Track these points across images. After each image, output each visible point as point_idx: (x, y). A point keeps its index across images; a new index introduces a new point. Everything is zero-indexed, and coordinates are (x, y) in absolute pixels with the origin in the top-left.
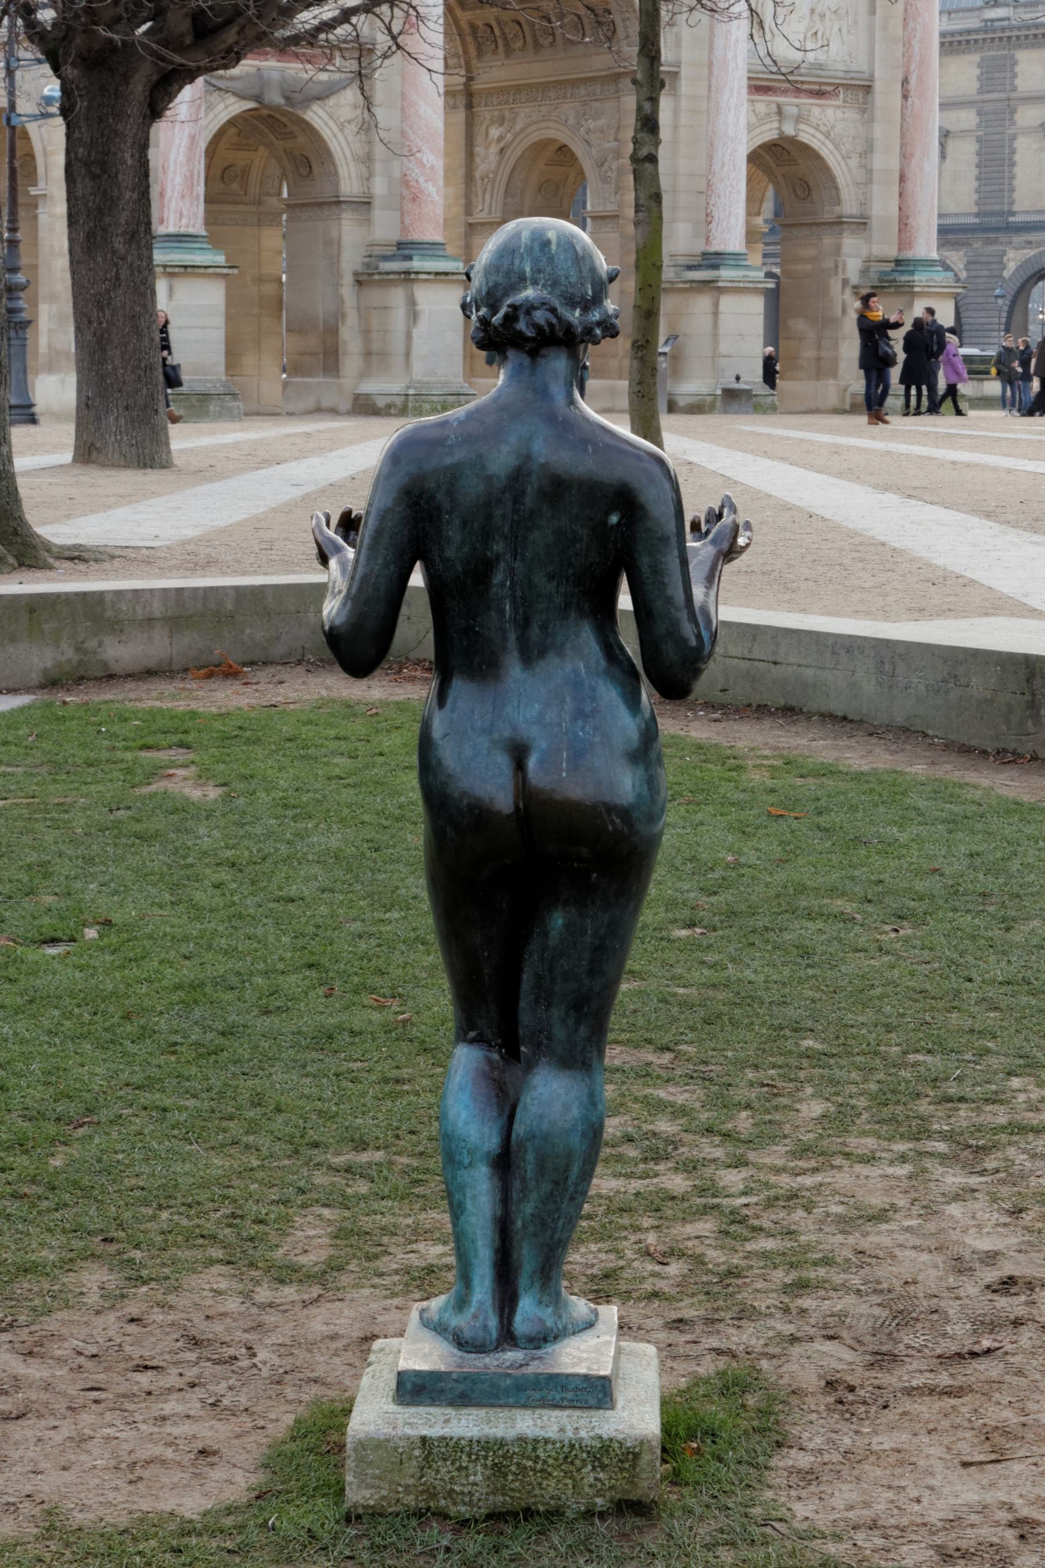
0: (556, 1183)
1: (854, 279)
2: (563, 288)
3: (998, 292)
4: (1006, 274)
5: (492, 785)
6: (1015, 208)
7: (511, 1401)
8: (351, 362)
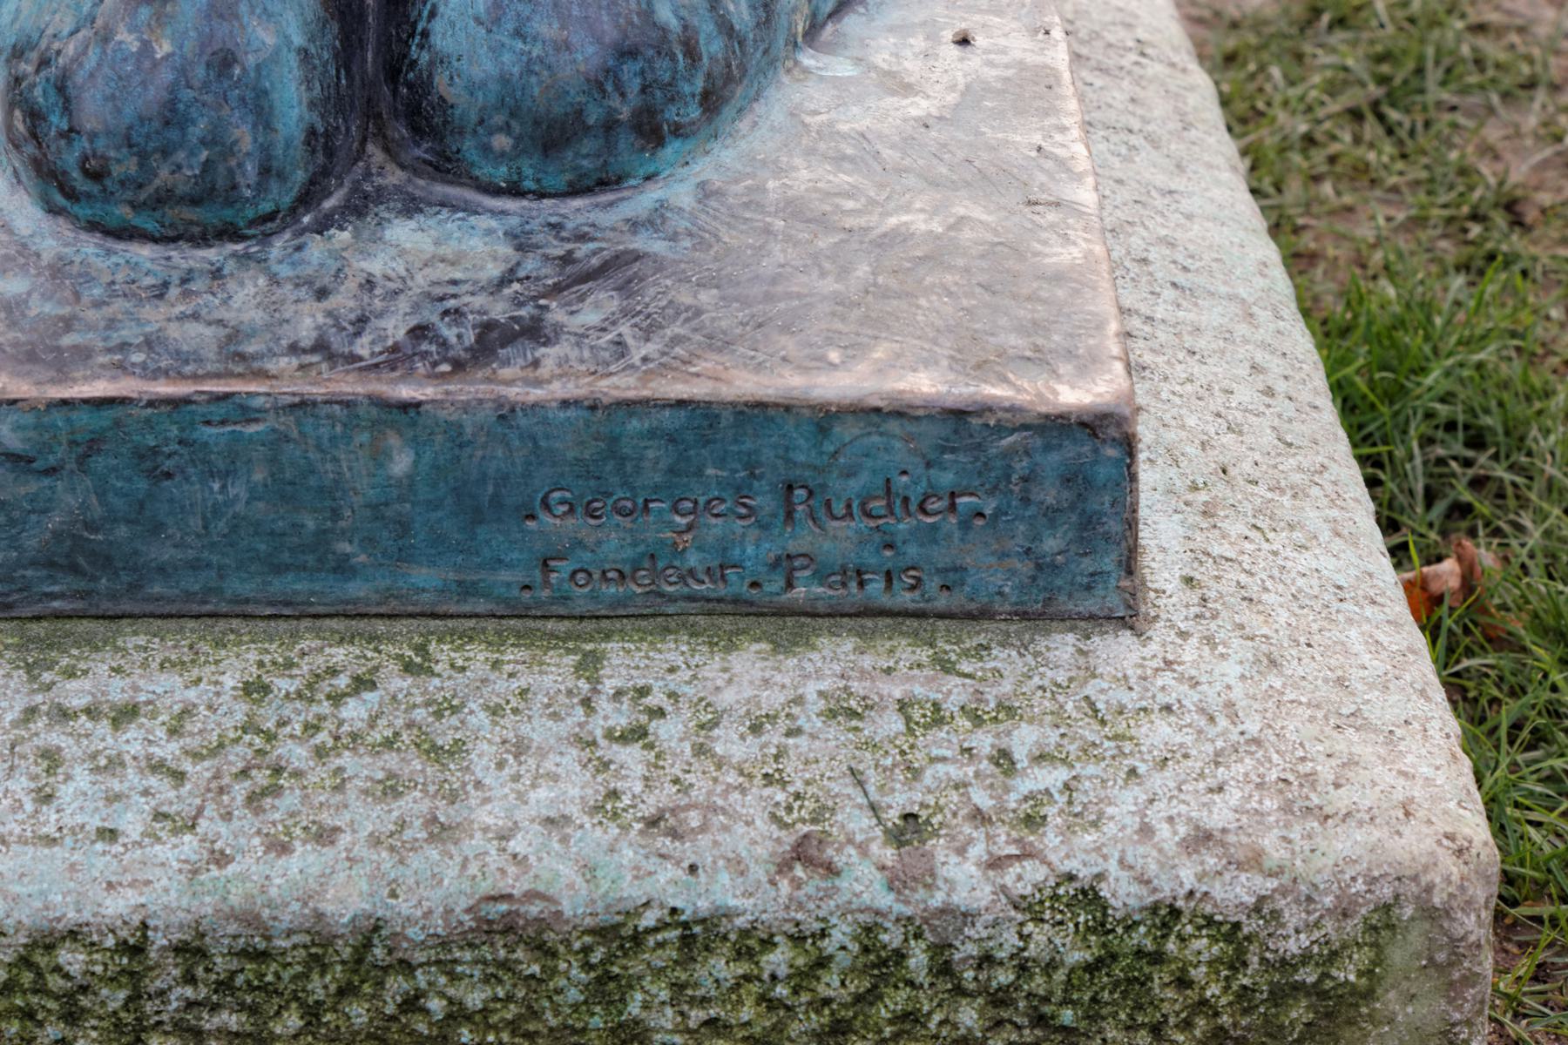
7: (425, 577)
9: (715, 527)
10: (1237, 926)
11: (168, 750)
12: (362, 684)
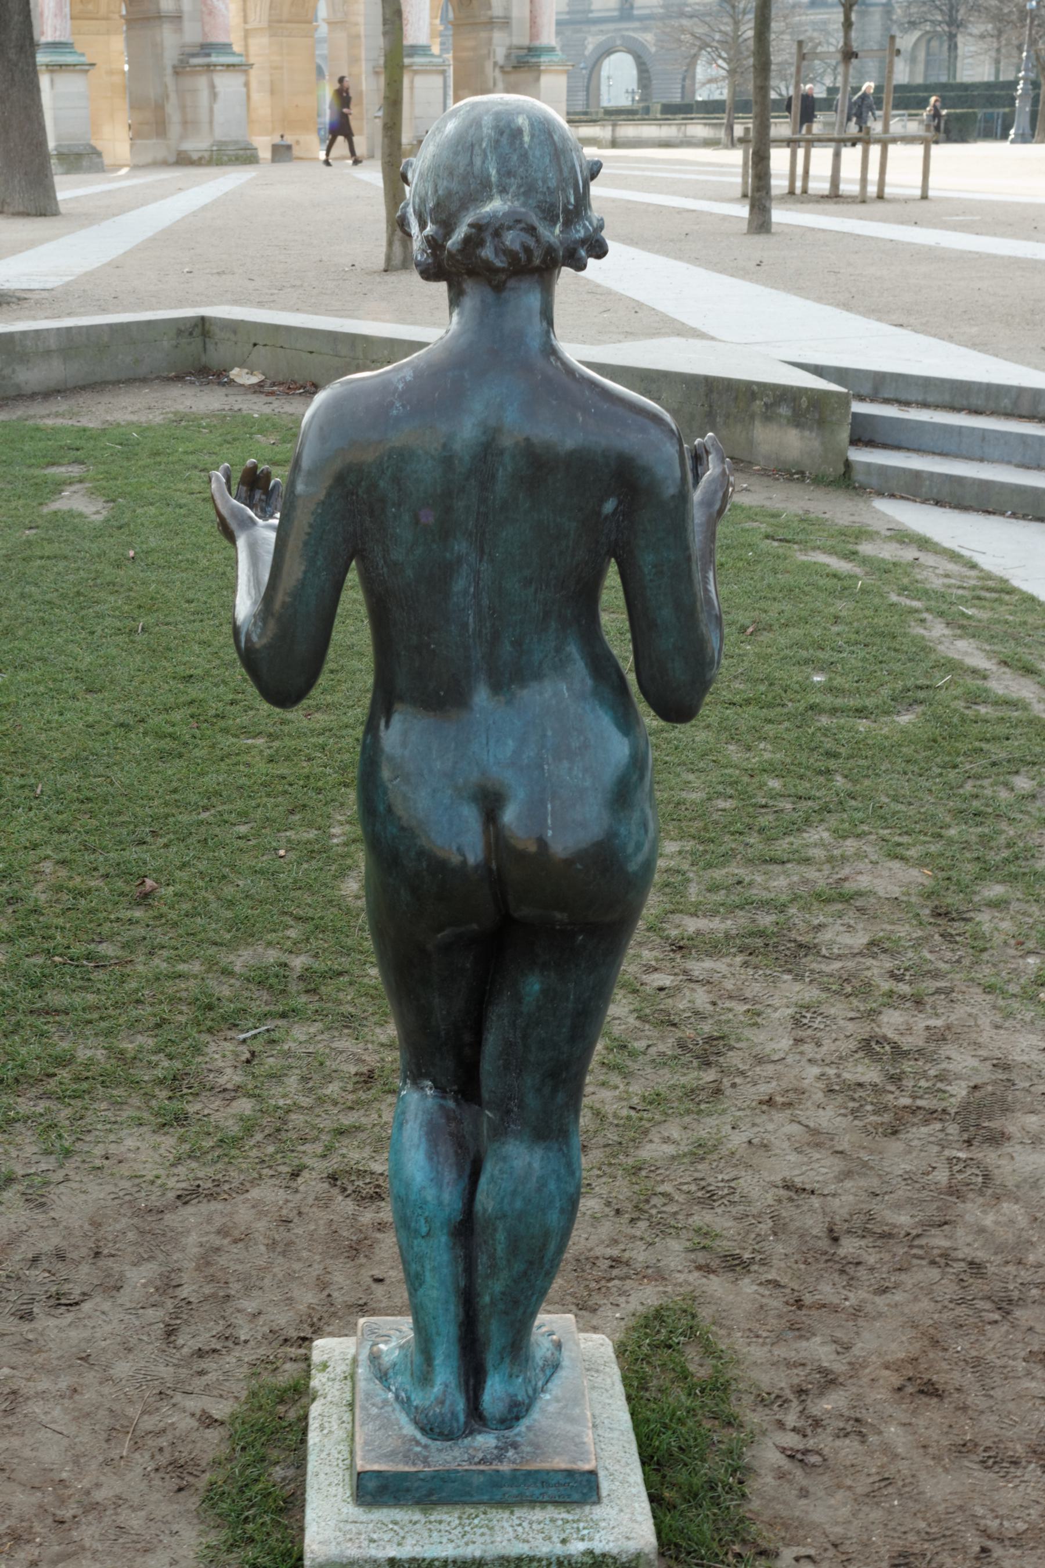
0: (531, 1263)
2: (540, 197)
4: (587, 53)
5: (458, 837)
6: (593, 7)
7: (485, 1498)
8: (175, 130)
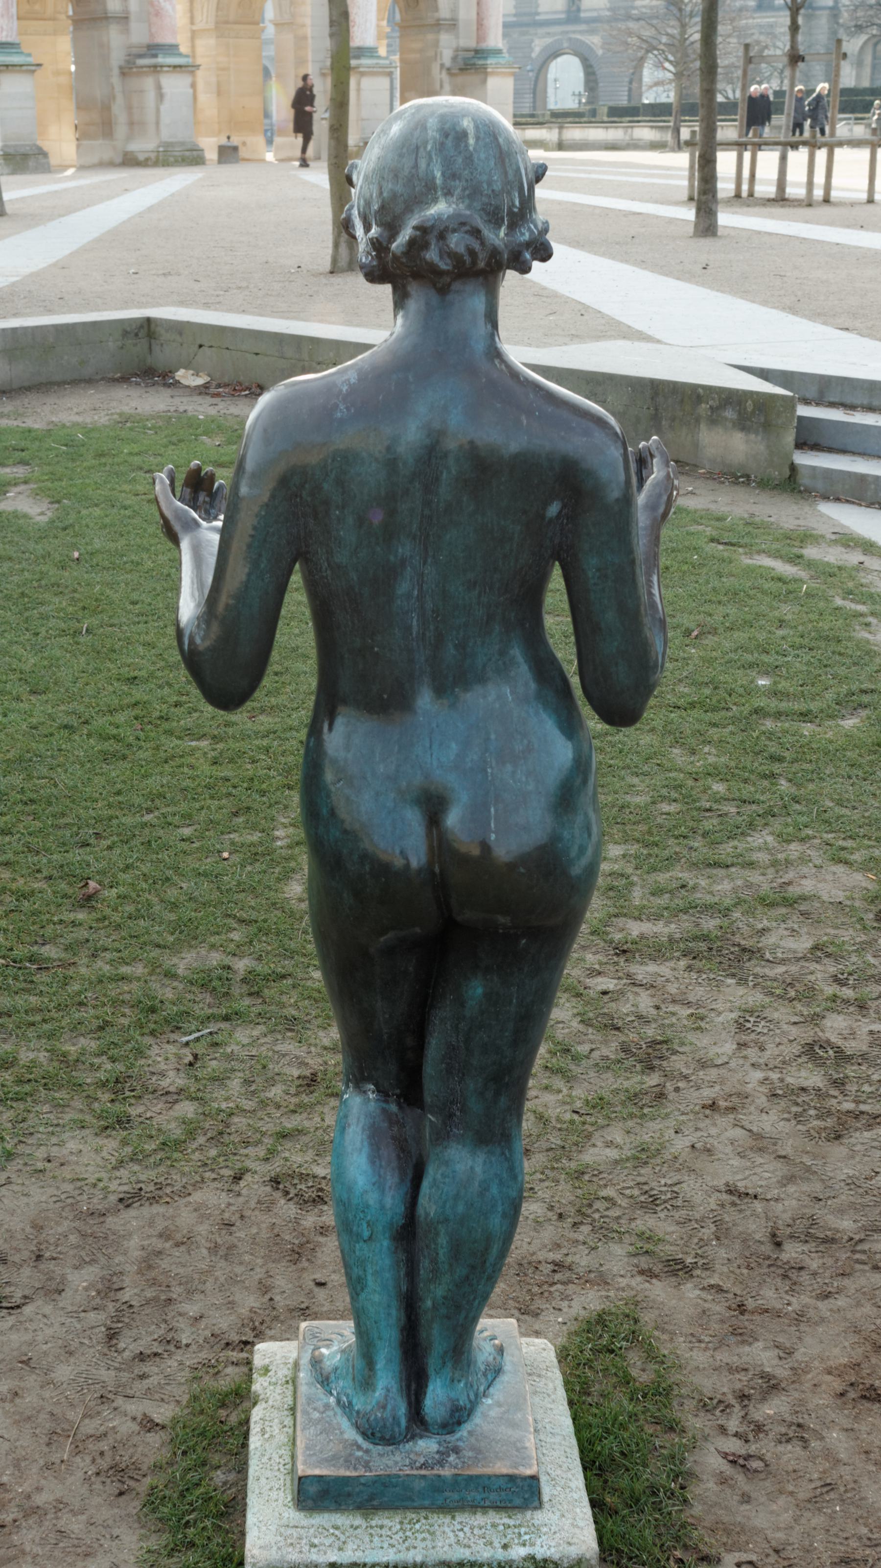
0: (473, 1267)
1: (448, 63)
3: (529, 68)
4: (534, 55)
6: (540, 10)
7: (427, 1503)
8: (121, 130)
9: (472, 1494)
10: (268, 1150)
11: (389, 1533)
12: (418, 1521)
